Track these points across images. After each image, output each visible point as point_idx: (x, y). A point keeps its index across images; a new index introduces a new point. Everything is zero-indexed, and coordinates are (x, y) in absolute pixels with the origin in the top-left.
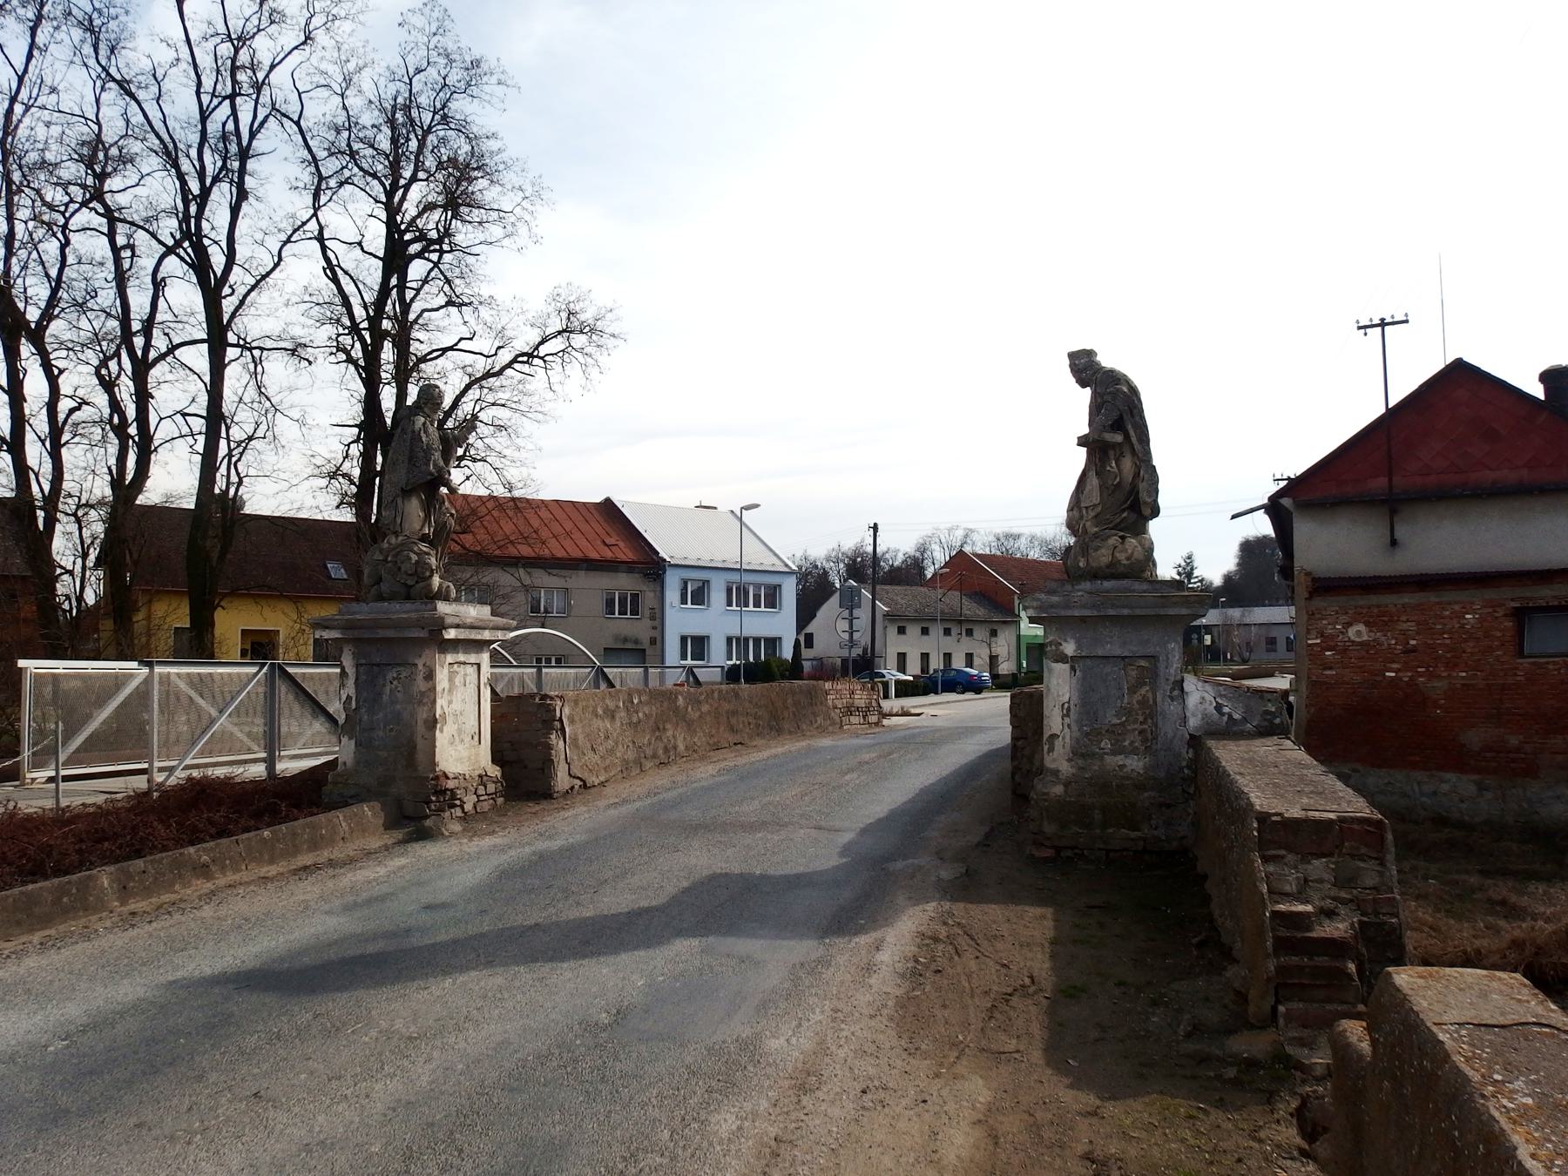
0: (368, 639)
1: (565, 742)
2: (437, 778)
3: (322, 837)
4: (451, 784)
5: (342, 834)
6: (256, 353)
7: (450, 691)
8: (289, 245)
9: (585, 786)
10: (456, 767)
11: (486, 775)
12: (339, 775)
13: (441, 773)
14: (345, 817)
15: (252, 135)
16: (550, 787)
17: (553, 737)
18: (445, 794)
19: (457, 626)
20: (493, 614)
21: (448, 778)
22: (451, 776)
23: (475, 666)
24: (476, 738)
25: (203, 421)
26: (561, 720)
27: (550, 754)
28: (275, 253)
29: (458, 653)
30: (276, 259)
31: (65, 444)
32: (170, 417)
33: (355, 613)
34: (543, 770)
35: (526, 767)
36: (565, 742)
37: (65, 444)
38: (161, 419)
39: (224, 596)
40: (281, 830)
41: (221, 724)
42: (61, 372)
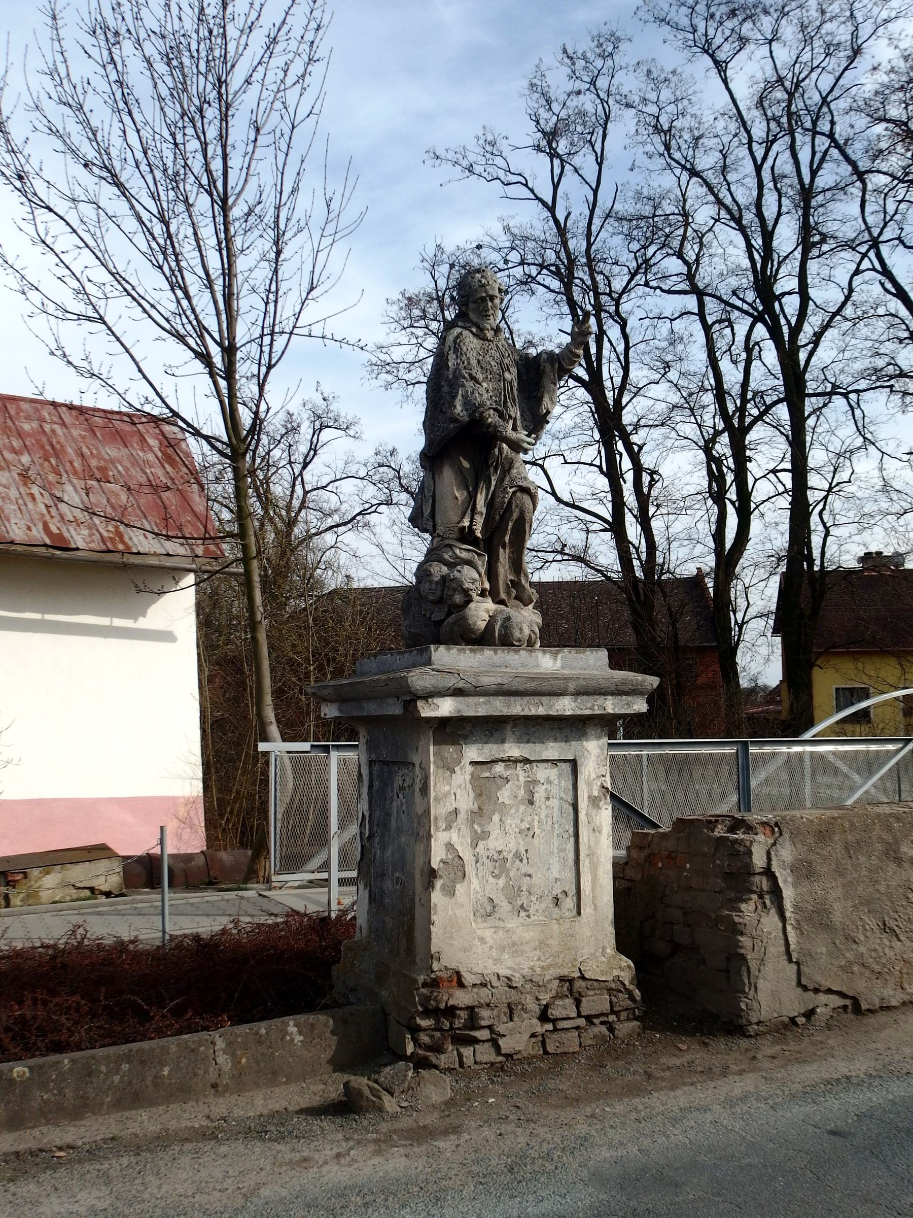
0: (527, 718)
1: (783, 918)
2: (434, 983)
3: (157, 1081)
4: (461, 998)
5: (212, 1076)
6: (853, 396)
7: (478, 814)
8: (295, 130)
9: (857, 1008)
10: (497, 961)
11: (583, 978)
12: (355, 942)
13: (444, 975)
14: (230, 1044)
15: (814, 173)
16: (738, 1013)
17: (748, 908)
18: (454, 1016)
19: (458, 692)
20: (614, 664)
21: (461, 985)
22: (468, 979)
23: (567, 767)
24: (569, 903)
25: (790, 474)
26: (768, 872)
27: (737, 945)
28: (845, 284)
29: (503, 741)
30: (846, 291)
31: (653, 516)
32: (764, 476)
33: (363, 674)
34: (727, 971)
35: (704, 961)
36: (783, 918)
37: (653, 516)
38: (756, 480)
39: (820, 655)
40: (165, 1050)
41: (866, 792)
42: (641, 448)
